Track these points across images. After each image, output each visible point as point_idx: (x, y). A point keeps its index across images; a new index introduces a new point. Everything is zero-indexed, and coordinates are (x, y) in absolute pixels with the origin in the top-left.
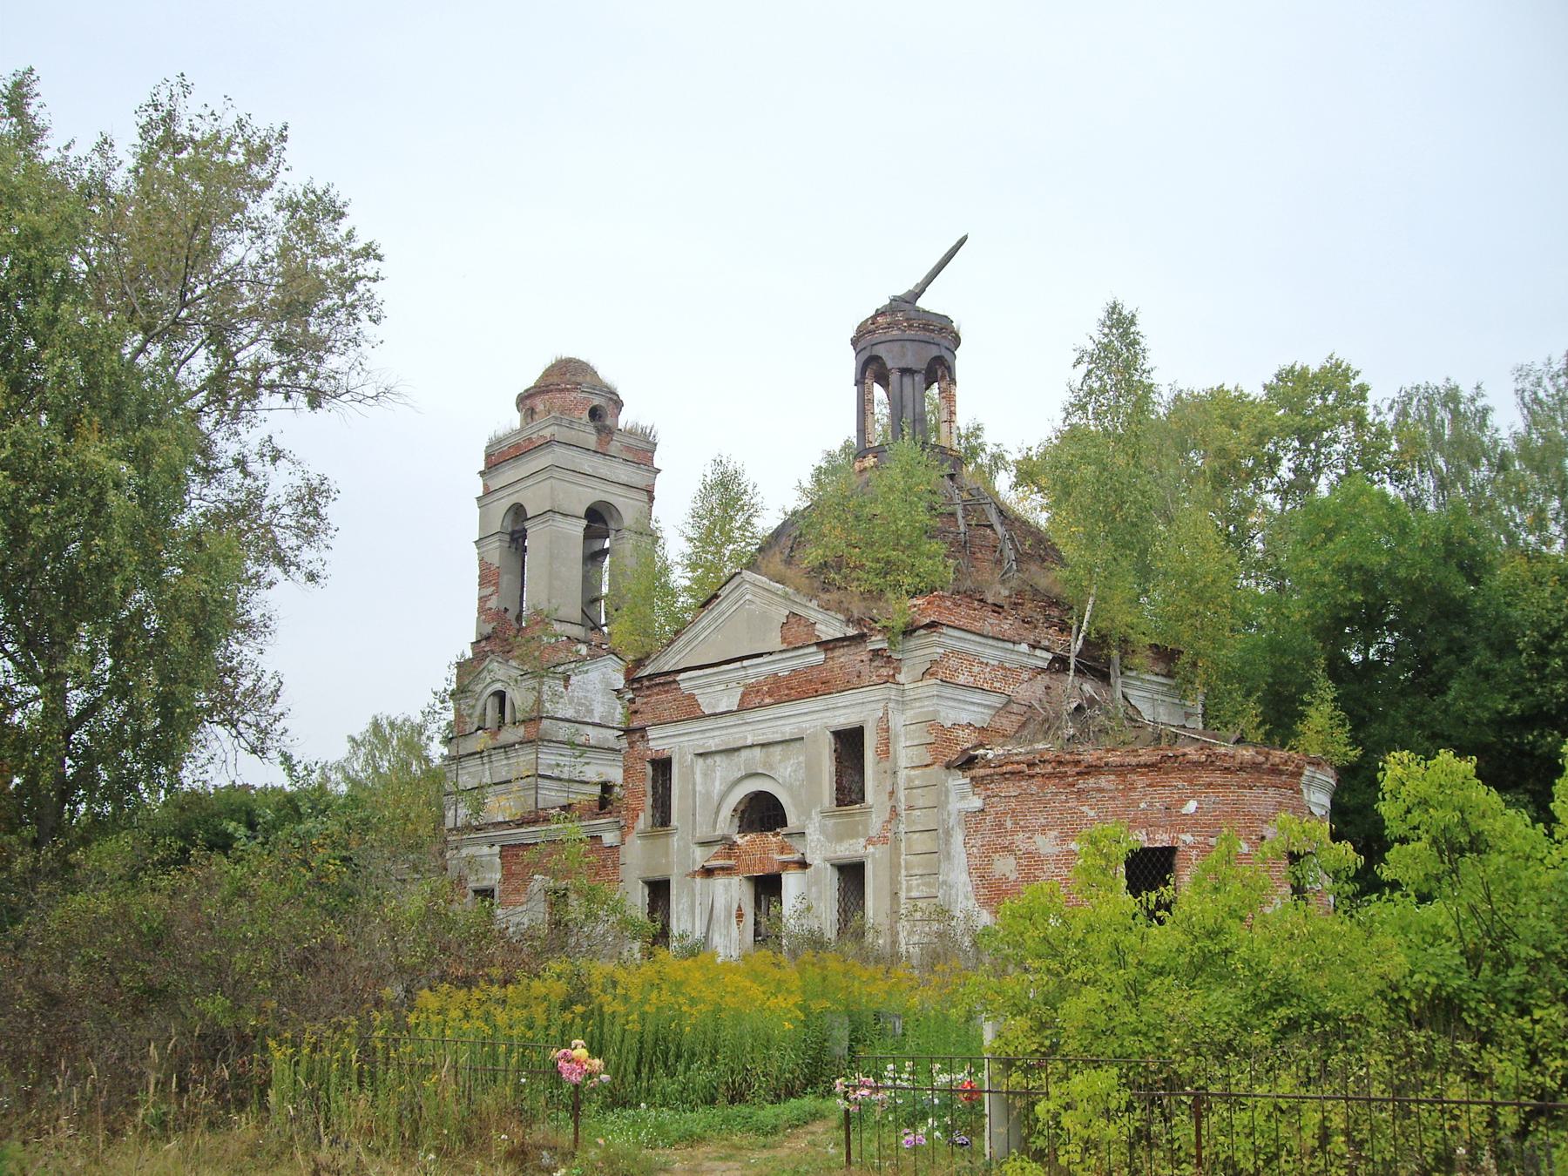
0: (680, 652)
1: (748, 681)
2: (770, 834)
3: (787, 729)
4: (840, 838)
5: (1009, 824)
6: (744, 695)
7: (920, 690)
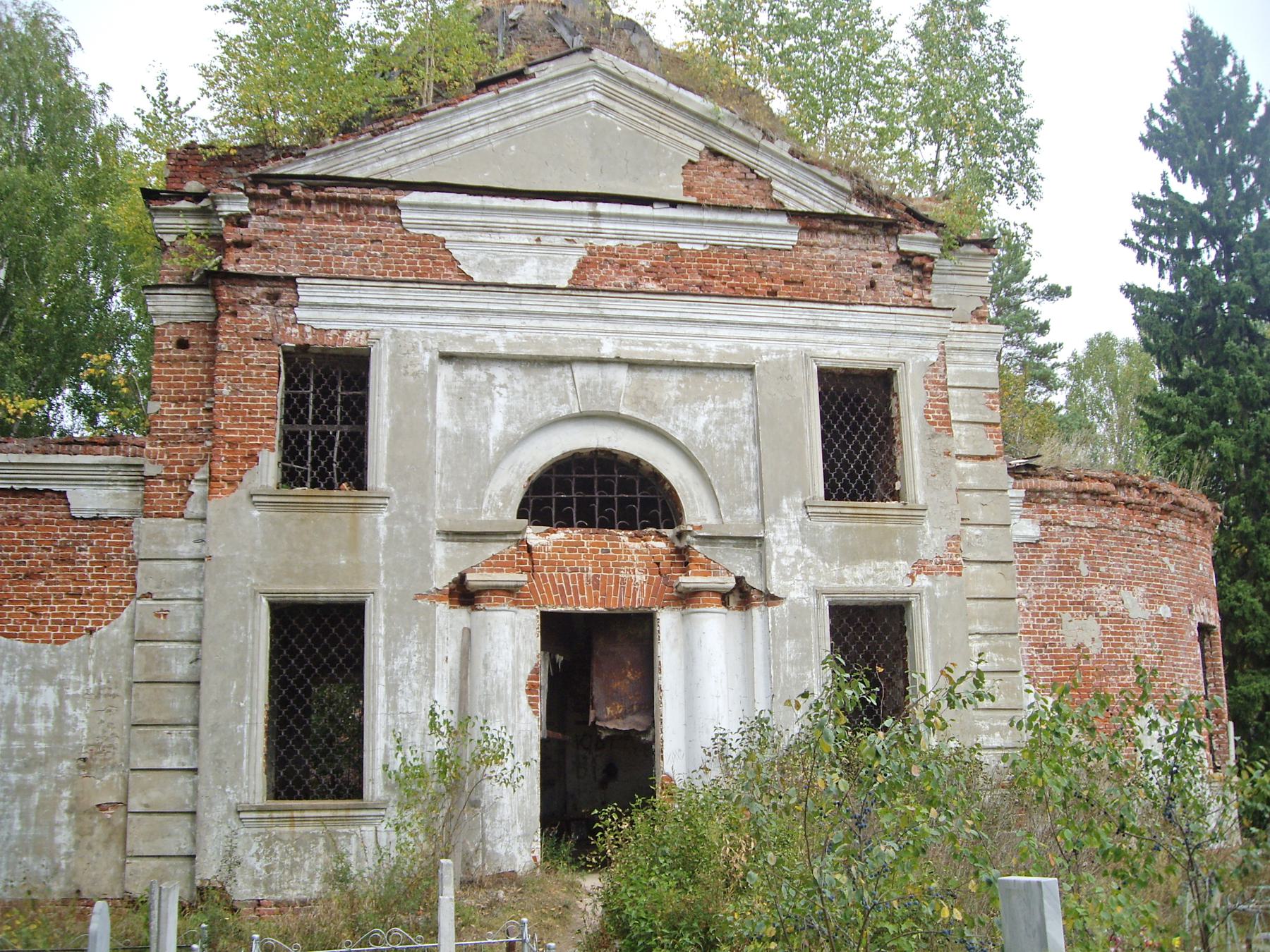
0: (400, 152)
1: (598, 243)
2: (624, 537)
3: (712, 345)
4: (852, 556)
5: (1084, 569)
6: (583, 266)
7: (972, 337)
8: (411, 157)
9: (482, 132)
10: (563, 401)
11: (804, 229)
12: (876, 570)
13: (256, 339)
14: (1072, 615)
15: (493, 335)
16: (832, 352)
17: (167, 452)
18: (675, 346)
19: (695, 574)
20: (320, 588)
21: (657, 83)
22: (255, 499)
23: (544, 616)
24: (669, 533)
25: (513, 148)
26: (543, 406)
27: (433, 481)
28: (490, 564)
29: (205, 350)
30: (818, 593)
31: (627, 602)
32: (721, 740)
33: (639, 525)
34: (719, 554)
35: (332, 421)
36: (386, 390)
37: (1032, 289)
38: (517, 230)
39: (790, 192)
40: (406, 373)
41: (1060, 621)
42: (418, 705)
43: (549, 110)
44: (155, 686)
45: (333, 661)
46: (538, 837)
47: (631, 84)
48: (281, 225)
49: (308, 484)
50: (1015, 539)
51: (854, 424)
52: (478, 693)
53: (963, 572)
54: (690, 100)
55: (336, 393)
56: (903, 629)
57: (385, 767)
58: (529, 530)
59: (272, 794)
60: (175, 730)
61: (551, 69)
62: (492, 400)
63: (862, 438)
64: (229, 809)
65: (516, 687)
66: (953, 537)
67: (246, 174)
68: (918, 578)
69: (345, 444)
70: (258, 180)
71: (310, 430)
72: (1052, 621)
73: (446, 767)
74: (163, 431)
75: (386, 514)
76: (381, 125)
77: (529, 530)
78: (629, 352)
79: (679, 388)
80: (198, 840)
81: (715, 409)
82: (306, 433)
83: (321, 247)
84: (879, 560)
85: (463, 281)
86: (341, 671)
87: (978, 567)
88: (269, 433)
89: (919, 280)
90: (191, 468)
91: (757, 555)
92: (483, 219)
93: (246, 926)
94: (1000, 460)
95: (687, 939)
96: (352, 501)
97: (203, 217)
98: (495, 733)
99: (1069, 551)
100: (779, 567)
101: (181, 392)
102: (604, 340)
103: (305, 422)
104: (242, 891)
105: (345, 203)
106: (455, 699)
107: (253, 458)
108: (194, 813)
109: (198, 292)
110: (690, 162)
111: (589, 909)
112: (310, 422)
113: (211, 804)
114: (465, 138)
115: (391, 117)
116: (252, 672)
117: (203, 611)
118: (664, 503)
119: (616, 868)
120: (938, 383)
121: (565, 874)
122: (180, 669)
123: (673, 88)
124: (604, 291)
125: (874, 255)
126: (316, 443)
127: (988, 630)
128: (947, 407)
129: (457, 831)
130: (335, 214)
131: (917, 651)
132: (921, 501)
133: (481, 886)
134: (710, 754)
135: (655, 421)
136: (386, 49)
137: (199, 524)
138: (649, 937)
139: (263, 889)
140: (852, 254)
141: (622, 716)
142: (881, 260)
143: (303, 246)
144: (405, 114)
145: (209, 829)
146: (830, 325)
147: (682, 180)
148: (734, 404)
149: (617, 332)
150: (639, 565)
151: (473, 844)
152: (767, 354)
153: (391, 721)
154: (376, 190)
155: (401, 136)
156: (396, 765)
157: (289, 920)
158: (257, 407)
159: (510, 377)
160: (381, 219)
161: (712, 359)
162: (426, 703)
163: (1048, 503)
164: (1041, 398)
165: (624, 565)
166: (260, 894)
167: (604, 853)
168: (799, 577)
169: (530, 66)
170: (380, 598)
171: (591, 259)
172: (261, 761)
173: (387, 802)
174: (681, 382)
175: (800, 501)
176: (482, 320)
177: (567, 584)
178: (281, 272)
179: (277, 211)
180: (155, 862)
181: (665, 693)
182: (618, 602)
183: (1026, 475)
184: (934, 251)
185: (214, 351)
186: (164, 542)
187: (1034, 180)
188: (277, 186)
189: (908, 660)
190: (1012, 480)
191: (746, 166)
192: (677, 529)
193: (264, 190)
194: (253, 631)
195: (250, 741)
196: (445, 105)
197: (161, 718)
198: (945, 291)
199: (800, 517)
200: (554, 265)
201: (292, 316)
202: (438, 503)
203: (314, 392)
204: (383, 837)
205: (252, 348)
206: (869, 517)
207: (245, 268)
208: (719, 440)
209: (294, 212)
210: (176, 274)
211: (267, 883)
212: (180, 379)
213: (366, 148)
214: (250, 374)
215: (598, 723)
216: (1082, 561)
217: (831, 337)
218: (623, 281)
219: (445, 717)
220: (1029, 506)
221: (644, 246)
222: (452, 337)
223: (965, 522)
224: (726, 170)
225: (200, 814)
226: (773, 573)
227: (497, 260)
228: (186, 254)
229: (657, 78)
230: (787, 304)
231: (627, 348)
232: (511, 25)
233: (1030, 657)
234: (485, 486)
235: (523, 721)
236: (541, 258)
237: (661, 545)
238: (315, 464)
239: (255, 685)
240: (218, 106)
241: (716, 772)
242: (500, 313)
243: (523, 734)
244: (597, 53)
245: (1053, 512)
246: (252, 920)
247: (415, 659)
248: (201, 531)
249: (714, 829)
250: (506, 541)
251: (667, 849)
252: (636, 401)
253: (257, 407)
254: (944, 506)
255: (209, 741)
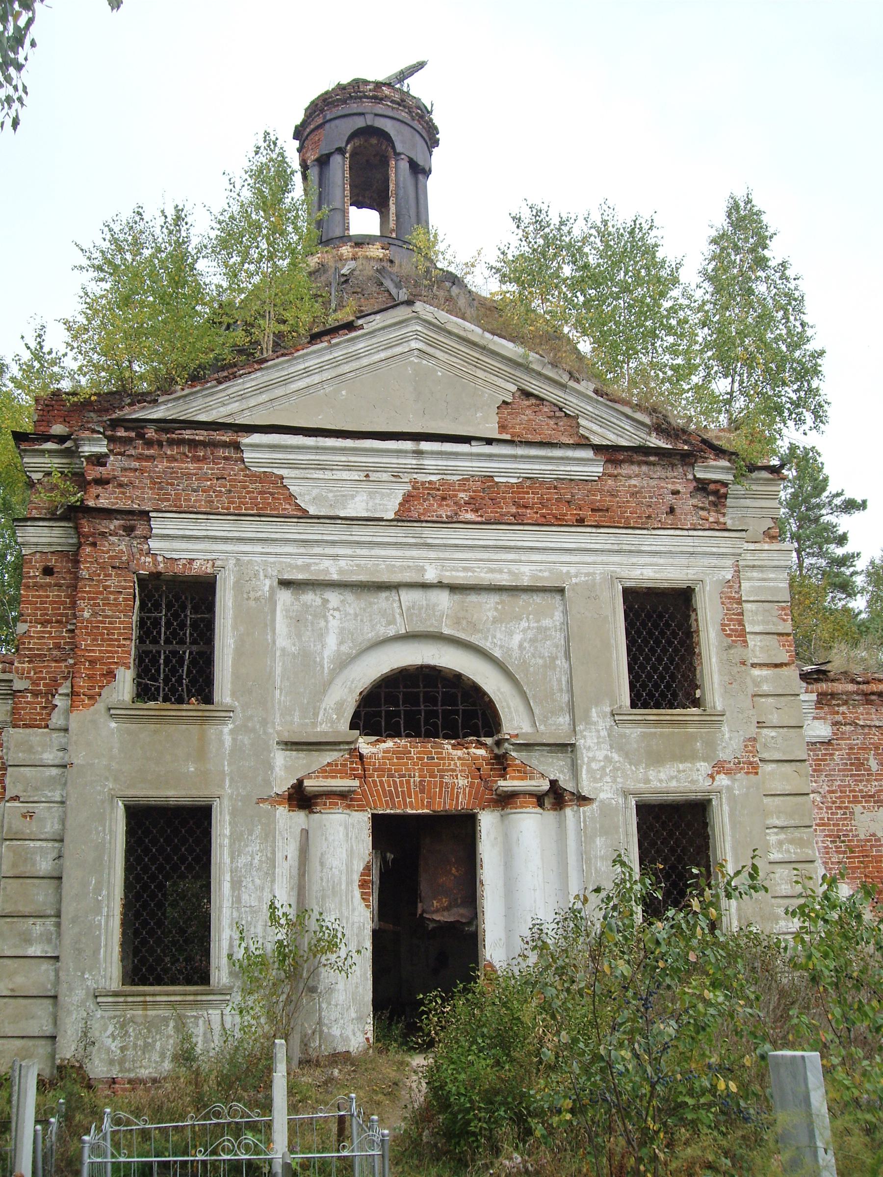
0: (242, 397)
1: (421, 478)
2: (447, 746)
3: (526, 569)
4: (656, 759)
6: (408, 499)
7: (764, 555)
8: (252, 402)
9: (316, 379)
10: (390, 623)
11: (608, 461)
12: (679, 771)
13: (113, 567)
14: (864, 807)
15: (327, 563)
16: (636, 573)
17: (34, 668)
18: (492, 571)
19: (513, 778)
20: (171, 793)
21: (474, 331)
22: (112, 712)
23: (375, 818)
24: (489, 741)
25: (344, 393)
26: (373, 627)
27: (274, 696)
28: (326, 771)
29: (68, 576)
30: (626, 794)
31: (451, 805)
32: (538, 928)
33: (461, 734)
34: (535, 760)
35: (182, 642)
36: (230, 614)
37: (830, 503)
38: (348, 468)
39: (595, 428)
40: (248, 599)
41: (852, 813)
42: (260, 899)
43: (377, 357)
44: (21, 880)
45: (183, 859)
46: (370, 1020)
47: (450, 333)
48: (136, 464)
49: (161, 699)
50: (808, 739)
51: (657, 638)
52: (315, 888)
53: (760, 771)
54: (503, 346)
55: (186, 616)
56: (705, 825)
57: (230, 956)
58: (361, 740)
59: (128, 980)
60: (39, 921)
61: (378, 321)
62: (327, 621)
63: (664, 651)
64: (87, 994)
65: (349, 882)
66: (750, 739)
67: (105, 419)
68: (717, 777)
69: (193, 662)
70: (115, 424)
71: (163, 650)
72: (845, 814)
73: (285, 956)
74: (30, 649)
75: (231, 726)
76: (225, 374)
77: (361, 740)
78: (450, 577)
79: (496, 609)
80: (58, 1023)
81: (529, 628)
82: (159, 653)
83: (172, 484)
84: (681, 762)
85: (299, 514)
86: (190, 868)
87: (774, 765)
88: (125, 652)
89: (714, 504)
90: (55, 684)
91: (569, 760)
92: (318, 457)
93: (100, 1103)
94: (793, 667)
95: (502, 1113)
96: (199, 714)
97: (66, 457)
98: (329, 924)
99: (859, 749)
100: (590, 771)
101: (47, 614)
102: (427, 567)
103: (158, 642)
104: (98, 1069)
105: (193, 444)
106: (294, 893)
107: (110, 675)
108: (55, 997)
109: (62, 524)
110: (504, 402)
111: (414, 1085)
112: (162, 642)
113: (71, 989)
114: (301, 384)
115: (235, 365)
116: (109, 868)
117: (65, 813)
118: (484, 714)
119: (440, 1048)
120: (733, 598)
121: (395, 1054)
122: (45, 866)
123: (488, 335)
124: (427, 521)
125: (673, 483)
126: (167, 661)
127: (785, 824)
128: (742, 620)
129: (296, 1015)
130: (184, 454)
131: (718, 845)
132: (719, 707)
133: (318, 1064)
134: (527, 943)
135: (474, 639)
136: (231, 304)
137: (62, 734)
138: (468, 1111)
139: (117, 1067)
140: (653, 483)
141: (447, 909)
142: (679, 487)
143: (155, 483)
144: (247, 364)
145: (69, 1013)
146: (633, 548)
147: (497, 419)
148: (546, 622)
149: (439, 559)
150: (461, 771)
151: (310, 1026)
152: (576, 576)
153: (235, 914)
154: (221, 432)
155: (243, 383)
156: (240, 954)
157: (140, 1096)
158: (114, 629)
159: (342, 601)
160: (226, 458)
161: (526, 582)
162: (267, 897)
163: (838, 705)
164: (840, 604)
165: (448, 771)
166: (115, 1073)
167: (429, 1034)
168: (608, 779)
169: (358, 318)
170: (226, 802)
171: (415, 492)
172: (117, 949)
173: (231, 988)
174: (498, 603)
175: (608, 709)
176: (317, 550)
177: (396, 789)
178: (137, 506)
179: (132, 452)
180: (19, 1043)
181: (486, 887)
182: (443, 805)
183: (817, 680)
184: (728, 477)
185: (77, 578)
186: (30, 750)
187: (821, 406)
188: (132, 429)
189: (711, 854)
190: (805, 685)
191: (555, 405)
192: (496, 738)
193: (121, 433)
194: (111, 831)
195: (107, 932)
196: (283, 355)
197: (27, 910)
198: (739, 513)
199: (608, 725)
200: (382, 499)
201: (146, 547)
202: (278, 716)
203: (166, 615)
204: (228, 1019)
205: (110, 575)
206: (672, 723)
207: (103, 503)
208: (533, 656)
209: (147, 452)
210: (42, 508)
211: (122, 1062)
212: (45, 603)
213: (212, 394)
214: (108, 599)
215: (425, 915)
216: (871, 757)
217: (634, 560)
218: (445, 513)
219: (285, 910)
220: (822, 708)
221: (463, 479)
222: (290, 565)
223: (760, 724)
224: (537, 409)
225: (60, 998)
226: (584, 776)
227: (330, 495)
228: (52, 490)
229: (473, 327)
230: (594, 530)
231: (448, 574)
232: (343, 280)
233: (825, 848)
234: (321, 701)
235: (356, 913)
236: (370, 493)
237: (482, 752)
238: (167, 680)
239: (112, 881)
240: (80, 357)
241: (533, 958)
242: (333, 543)
243: (356, 925)
244: (419, 306)
245: (843, 713)
246: (107, 1096)
247: (257, 858)
248: (64, 740)
249: (529, 1011)
250: (340, 750)
251: (485, 1030)
252: (457, 622)
253: (114, 629)
254: (741, 711)
255: (69, 931)
